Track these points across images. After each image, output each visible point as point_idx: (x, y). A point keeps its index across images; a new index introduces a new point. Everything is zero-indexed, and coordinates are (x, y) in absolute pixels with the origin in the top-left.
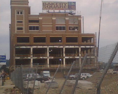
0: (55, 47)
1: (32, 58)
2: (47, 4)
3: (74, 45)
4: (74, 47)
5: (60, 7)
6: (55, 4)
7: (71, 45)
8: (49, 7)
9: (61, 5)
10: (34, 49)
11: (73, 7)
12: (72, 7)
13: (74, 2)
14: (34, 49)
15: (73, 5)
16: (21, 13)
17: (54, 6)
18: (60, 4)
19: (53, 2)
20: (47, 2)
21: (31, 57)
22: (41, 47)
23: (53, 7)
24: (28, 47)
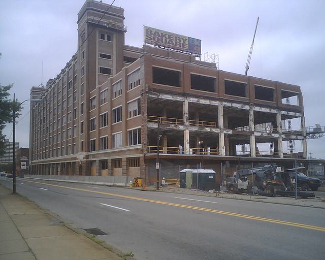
0: (234, 105)
1: (187, 130)
2: (153, 33)
3: (271, 107)
5: (176, 44)
6: (167, 36)
8: (156, 39)
9: (178, 41)
11: (197, 49)
12: (195, 48)
13: (198, 40)
15: (197, 45)
16: (109, 39)
17: (166, 40)
18: (176, 38)
19: (165, 32)
20: (154, 29)
21: (185, 126)
22: (207, 102)
23: (164, 42)
24: (179, 99)
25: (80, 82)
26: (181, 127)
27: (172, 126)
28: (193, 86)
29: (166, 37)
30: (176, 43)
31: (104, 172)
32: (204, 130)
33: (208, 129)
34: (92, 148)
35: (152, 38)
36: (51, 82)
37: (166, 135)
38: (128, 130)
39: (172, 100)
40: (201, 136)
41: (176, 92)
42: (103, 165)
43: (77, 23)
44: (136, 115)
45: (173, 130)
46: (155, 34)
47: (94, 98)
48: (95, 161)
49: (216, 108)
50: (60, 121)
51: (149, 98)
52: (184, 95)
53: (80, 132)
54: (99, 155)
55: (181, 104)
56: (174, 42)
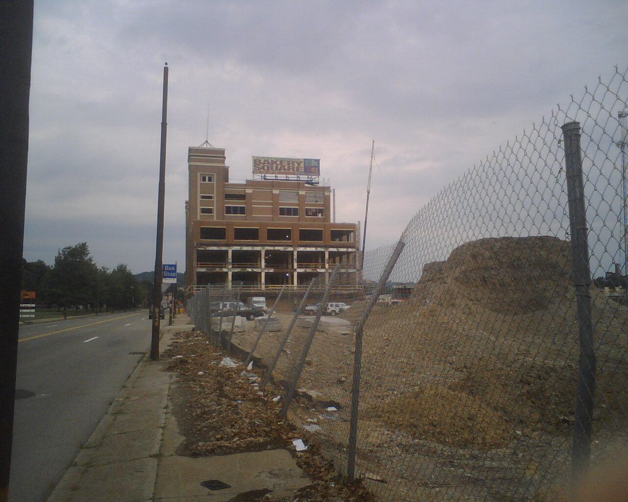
0: (277, 248)
1: (230, 271)
5: (289, 169)
9: (291, 165)
13: (316, 160)
15: (315, 166)
17: (277, 167)
19: (275, 158)
24: (224, 248)
27: (218, 270)
32: (246, 271)
33: (250, 270)
46: (264, 163)
51: (198, 250)
56: (286, 167)
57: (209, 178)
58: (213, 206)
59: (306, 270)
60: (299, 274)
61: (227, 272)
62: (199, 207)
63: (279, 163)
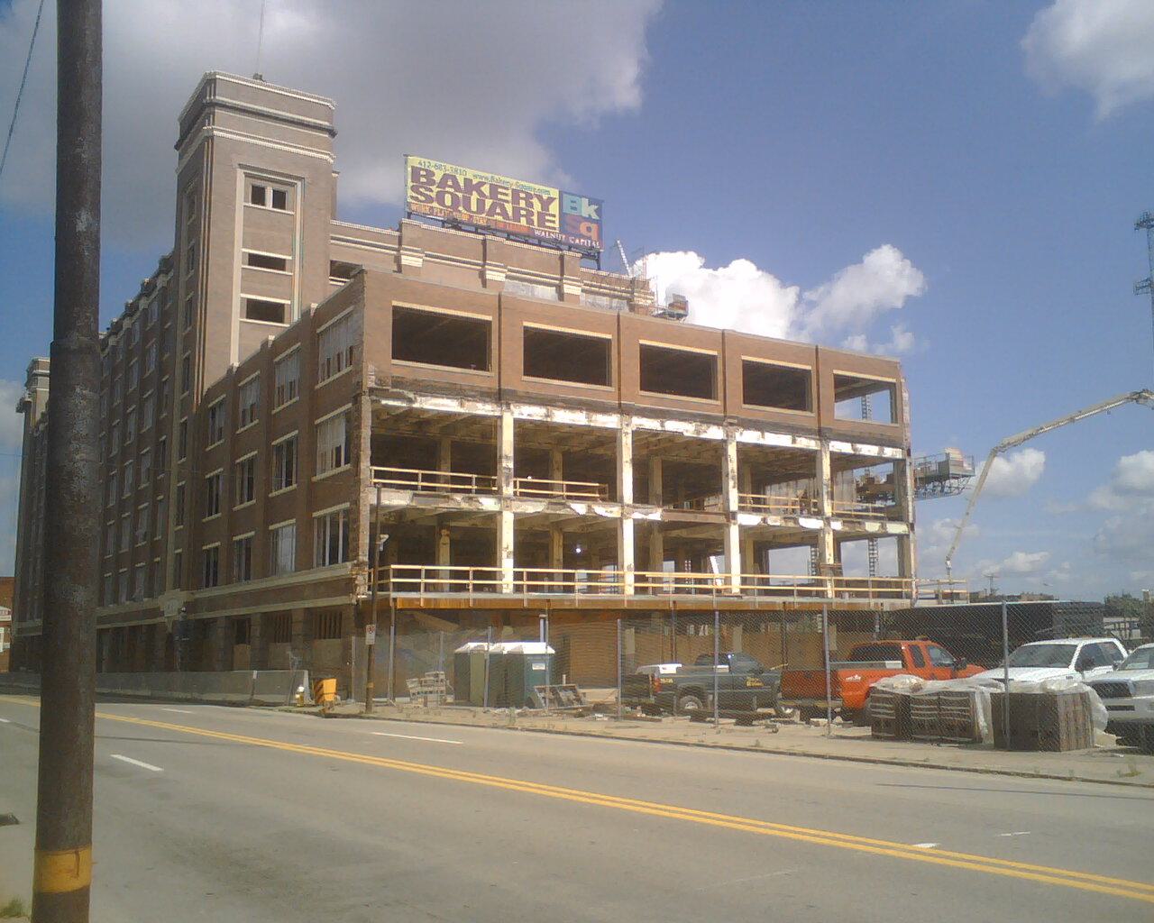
0: (672, 426)
1: (508, 508)
3: (795, 431)
4: (794, 441)
6: (486, 189)
7: (776, 428)
8: (448, 200)
9: (522, 204)
10: (524, 430)
11: (589, 229)
14: (524, 430)
15: (589, 219)
16: (280, 200)
17: (481, 203)
22: (578, 418)
23: (474, 207)
24: (484, 409)
25: (179, 347)
26: (488, 504)
27: (459, 502)
28: (532, 368)
29: (481, 194)
30: (516, 211)
31: (244, 651)
33: (580, 508)
34: (211, 504)
35: (433, 195)
36: (686, 251)
37: (449, 528)
38: (315, 515)
39: (460, 414)
40: (570, 529)
41: (472, 388)
42: (240, 629)
43: (177, 147)
44: (338, 464)
45: (461, 514)
46: (443, 184)
47: (221, 403)
48: (215, 620)
49: (609, 439)
50: (115, 484)
52: (501, 397)
53: (172, 520)
54: (231, 597)
55: (490, 428)
56: (509, 207)
57: (275, 192)
58: (291, 297)
59: (764, 520)
60: (744, 530)
61: (741, 527)
62: (239, 297)
63: (487, 193)
